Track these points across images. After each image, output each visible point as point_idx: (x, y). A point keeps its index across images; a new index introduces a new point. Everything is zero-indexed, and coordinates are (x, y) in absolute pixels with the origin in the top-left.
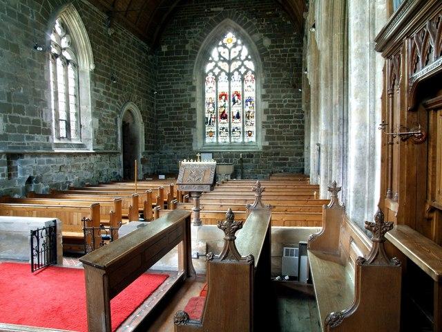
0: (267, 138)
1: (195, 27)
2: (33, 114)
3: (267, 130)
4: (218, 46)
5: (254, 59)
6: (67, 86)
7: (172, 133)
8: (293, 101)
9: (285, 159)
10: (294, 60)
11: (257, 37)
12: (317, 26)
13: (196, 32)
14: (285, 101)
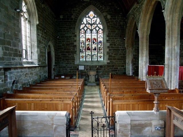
0: (109, 59)
1: (76, 8)
2: (15, 46)
3: (109, 56)
4: (86, 17)
5: (102, 24)
6: (26, 31)
7: (65, 56)
8: (120, 43)
9: (116, 68)
10: (120, 25)
11: (105, 14)
12: (165, 9)
13: (76, 10)
14: (117, 43)
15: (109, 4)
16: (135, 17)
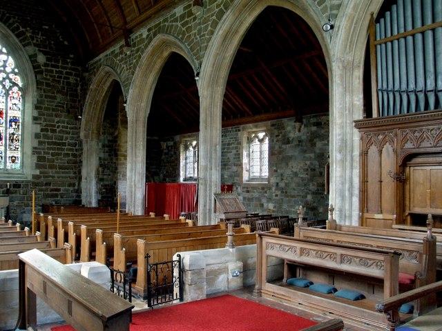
0: (38, 166)
3: (38, 157)
5: (22, 73)
8: (67, 127)
9: (57, 190)
10: (68, 84)
11: (31, 49)
14: (58, 127)
15: (44, 27)
16: (117, 73)
